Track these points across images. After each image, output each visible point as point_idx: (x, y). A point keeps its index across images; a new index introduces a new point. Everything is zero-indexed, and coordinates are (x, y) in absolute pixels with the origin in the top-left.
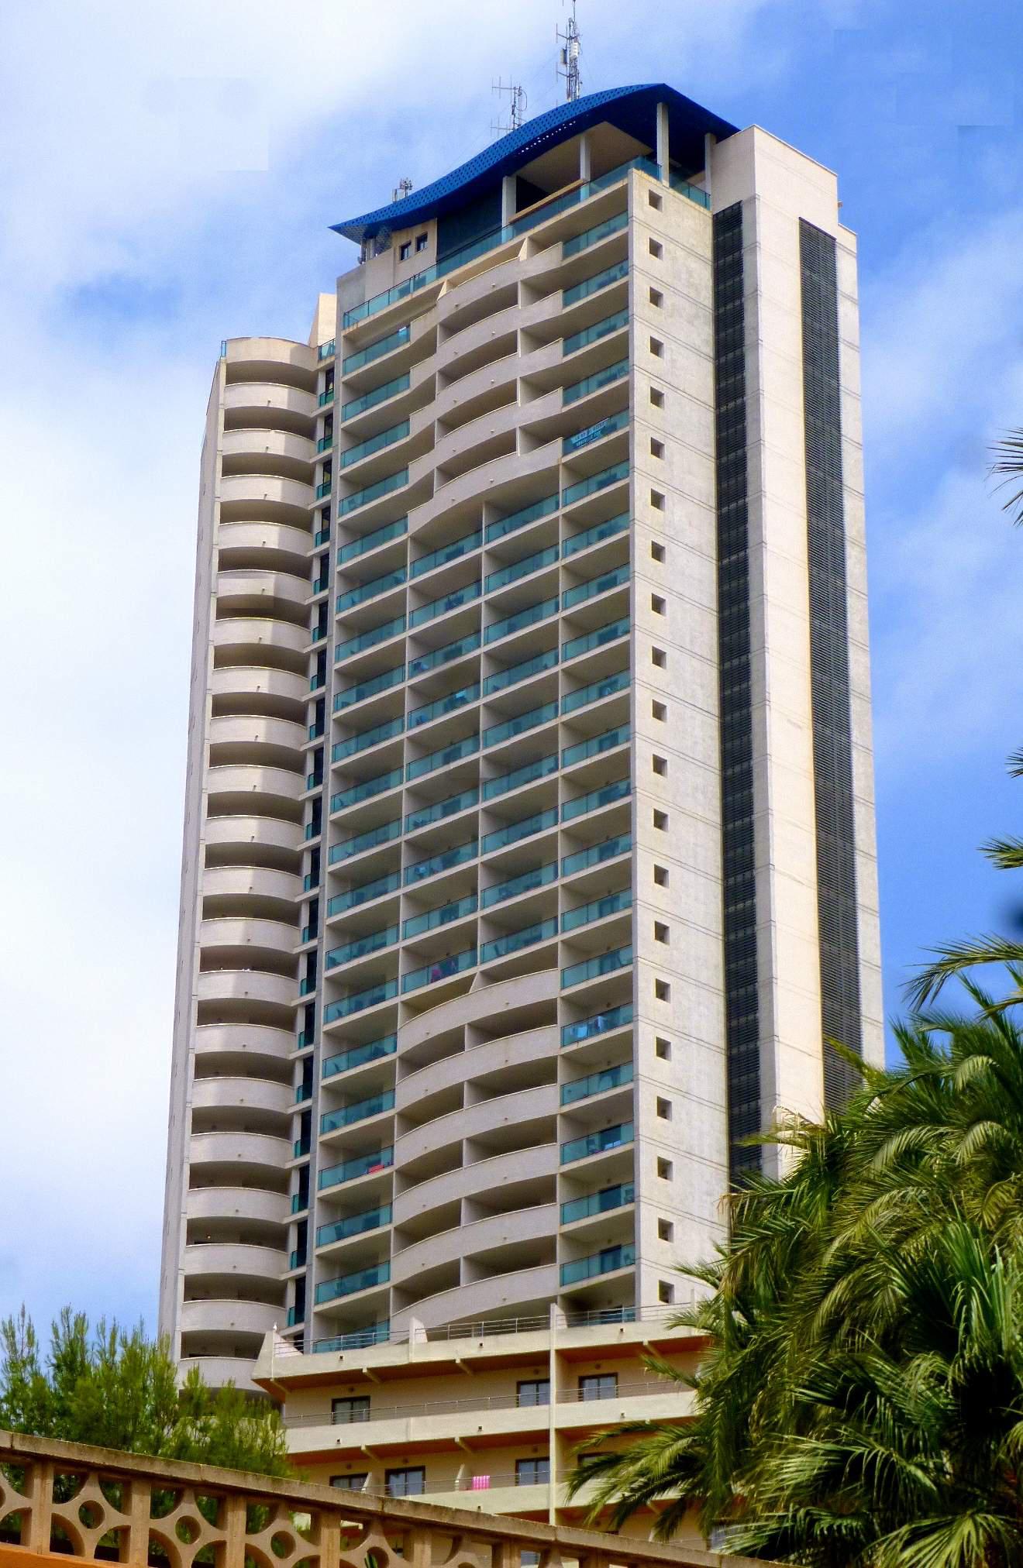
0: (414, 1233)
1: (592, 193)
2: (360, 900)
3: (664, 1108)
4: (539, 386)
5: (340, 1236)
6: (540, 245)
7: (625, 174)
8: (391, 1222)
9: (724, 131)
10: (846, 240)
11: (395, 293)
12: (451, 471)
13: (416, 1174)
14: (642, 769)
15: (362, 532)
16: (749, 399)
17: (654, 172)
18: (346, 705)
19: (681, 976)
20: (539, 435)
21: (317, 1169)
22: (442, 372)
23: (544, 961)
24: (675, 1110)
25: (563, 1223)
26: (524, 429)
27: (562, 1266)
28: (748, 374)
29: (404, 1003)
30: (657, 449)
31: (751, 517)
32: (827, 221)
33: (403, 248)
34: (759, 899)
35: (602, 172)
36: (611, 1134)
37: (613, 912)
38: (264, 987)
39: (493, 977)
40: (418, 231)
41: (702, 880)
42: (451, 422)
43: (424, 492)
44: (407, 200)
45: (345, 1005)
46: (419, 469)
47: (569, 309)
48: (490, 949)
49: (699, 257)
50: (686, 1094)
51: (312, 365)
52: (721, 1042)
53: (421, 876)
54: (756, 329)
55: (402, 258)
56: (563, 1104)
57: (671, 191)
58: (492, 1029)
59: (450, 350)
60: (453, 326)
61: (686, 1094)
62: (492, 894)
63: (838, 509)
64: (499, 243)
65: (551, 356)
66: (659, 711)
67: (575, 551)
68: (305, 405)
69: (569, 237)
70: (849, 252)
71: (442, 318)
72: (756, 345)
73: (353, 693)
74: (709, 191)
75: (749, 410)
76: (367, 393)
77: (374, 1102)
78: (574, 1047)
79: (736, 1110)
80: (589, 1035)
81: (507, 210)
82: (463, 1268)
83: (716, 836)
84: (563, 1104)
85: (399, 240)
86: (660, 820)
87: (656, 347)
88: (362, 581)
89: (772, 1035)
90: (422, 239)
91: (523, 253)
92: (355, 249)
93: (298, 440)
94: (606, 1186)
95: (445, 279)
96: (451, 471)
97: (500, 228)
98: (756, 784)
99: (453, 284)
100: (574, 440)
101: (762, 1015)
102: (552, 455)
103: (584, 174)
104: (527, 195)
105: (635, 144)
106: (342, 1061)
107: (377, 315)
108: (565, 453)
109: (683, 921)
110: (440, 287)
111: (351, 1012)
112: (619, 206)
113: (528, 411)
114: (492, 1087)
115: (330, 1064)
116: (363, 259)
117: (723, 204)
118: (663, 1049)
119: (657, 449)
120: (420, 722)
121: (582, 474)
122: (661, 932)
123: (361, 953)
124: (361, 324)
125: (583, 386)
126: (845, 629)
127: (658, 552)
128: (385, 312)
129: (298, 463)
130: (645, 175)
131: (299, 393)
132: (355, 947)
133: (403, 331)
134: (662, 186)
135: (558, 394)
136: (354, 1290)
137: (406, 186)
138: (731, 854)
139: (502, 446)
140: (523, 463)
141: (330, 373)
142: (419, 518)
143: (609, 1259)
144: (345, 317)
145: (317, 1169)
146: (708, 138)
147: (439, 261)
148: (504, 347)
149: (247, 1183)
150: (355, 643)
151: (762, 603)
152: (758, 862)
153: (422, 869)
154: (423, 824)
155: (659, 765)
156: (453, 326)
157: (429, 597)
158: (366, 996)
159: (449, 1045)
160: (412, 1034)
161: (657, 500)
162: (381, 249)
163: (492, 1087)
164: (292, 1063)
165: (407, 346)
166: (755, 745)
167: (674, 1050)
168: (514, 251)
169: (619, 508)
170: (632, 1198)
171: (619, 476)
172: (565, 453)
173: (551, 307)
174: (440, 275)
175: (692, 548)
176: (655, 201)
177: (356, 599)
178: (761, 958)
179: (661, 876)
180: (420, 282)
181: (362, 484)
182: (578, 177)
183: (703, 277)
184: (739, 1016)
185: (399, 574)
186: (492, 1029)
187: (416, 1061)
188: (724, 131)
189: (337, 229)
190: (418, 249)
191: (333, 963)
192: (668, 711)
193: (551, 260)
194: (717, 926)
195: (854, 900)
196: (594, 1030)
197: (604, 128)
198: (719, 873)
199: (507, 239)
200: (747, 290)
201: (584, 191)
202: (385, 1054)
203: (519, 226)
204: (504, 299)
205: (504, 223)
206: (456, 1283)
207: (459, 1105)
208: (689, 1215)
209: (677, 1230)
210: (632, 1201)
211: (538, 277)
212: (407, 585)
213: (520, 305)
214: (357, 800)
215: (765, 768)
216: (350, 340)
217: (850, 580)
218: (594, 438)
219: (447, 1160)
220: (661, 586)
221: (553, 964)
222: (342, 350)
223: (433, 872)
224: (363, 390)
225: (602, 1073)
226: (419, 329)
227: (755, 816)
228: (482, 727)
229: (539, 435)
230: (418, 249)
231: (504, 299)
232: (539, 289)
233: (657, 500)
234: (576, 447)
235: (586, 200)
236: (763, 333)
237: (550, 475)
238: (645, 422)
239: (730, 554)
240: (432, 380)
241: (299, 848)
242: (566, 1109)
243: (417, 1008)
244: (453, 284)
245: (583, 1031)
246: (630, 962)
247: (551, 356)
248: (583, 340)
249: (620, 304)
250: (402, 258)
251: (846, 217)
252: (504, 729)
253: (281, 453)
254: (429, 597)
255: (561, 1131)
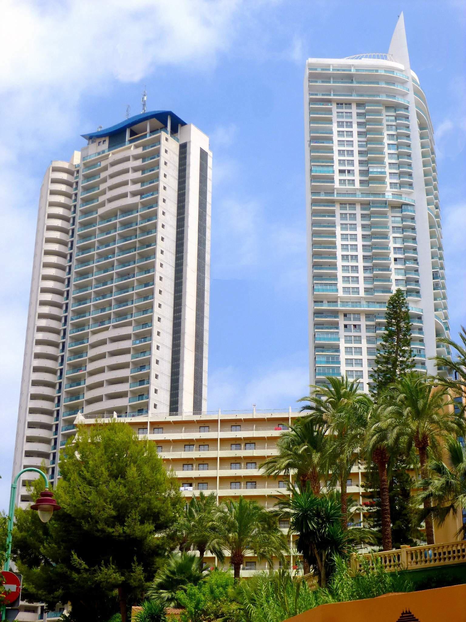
0: (91, 388)
1: (150, 136)
2: (80, 305)
3: (157, 362)
4: (135, 182)
5: (71, 387)
6: (136, 147)
7: (160, 132)
8: (87, 356)
9: (183, 124)
10: (210, 154)
11: (97, 154)
12: (110, 200)
13: (92, 373)
14: (157, 279)
15: (85, 213)
16: (183, 280)
17: (167, 133)
18: (78, 255)
19: (164, 303)
20: (134, 194)
21: (66, 370)
22: (108, 187)
23: (129, 324)
24: (160, 362)
25: (130, 388)
26: (132, 168)
27: (130, 384)
28: (186, 184)
29: (91, 331)
30: (164, 201)
31: (186, 219)
32: (206, 149)
33: (99, 143)
34: (182, 313)
35: (153, 132)
36: (143, 367)
37: (146, 314)
38: (54, 324)
39: (115, 327)
40: (103, 139)
41: (171, 254)
42: (111, 188)
43: (103, 204)
44: (101, 131)
45: (74, 331)
46: (101, 199)
47: (144, 175)
48: (114, 320)
49: (175, 154)
50: (162, 359)
51: (73, 169)
52: (170, 361)
53: (97, 300)
54: (189, 173)
55: (99, 145)
56: (132, 359)
57: (171, 138)
58: (114, 340)
59: (112, 170)
60: (113, 164)
61: (162, 359)
62: (116, 306)
63: (205, 244)
64: (125, 145)
65: (138, 175)
66: (161, 265)
67: (142, 224)
68: (71, 179)
69: (144, 147)
70: (211, 157)
71: (110, 162)
72: (189, 178)
73: (81, 253)
74: (179, 138)
75: (186, 194)
76: (88, 178)
77: (83, 328)
78: (135, 346)
79: (173, 364)
80: (139, 343)
81: (128, 137)
82: (106, 368)
83: (173, 297)
84: (132, 359)
85: (98, 140)
86: (160, 292)
87: (165, 176)
88: (84, 225)
89: (184, 346)
90: (104, 141)
91: (132, 148)
92: (86, 141)
93: (68, 199)
94: (142, 365)
95: (111, 152)
96: (110, 200)
97: (125, 141)
98: (186, 196)
99: (113, 154)
100: (143, 196)
101: (181, 341)
102: (137, 199)
103: (148, 130)
104: (133, 133)
105: (162, 125)
106: (78, 278)
107: (92, 159)
108: (141, 199)
109: (164, 317)
110: (109, 155)
111: (76, 332)
112: (158, 141)
113: (132, 188)
114: (113, 354)
115: (72, 331)
116: (88, 144)
117: (182, 142)
118: (158, 348)
119: (164, 201)
120: (98, 262)
121: (145, 205)
122: (159, 319)
123: (79, 318)
124: (88, 160)
125: (147, 147)
126: (205, 249)
127: (163, 226)
128: (94, 158)
129: (66, 229)
130: (165, 133)
131: (68, 187)
132: (78, 316)
133: (99, 163)
134: (169, 136)
135: (139, 184)
136: (73, 400)
137: (101, 127)
138: (176, 302)
139: (125, 196)
140: (129, 201)
141: (78, 172)
142: (101, 211)
143: (141, 397)
144: (83, 158)
145: (66, 370)
146: (179, 125)
147: (109, 147)
148: (126, 171)
149: (48, 345)
150: (83, 228)
151: (187, 241)
152: (180, 388)
153: (97, 298)
154: (98, 287)
155: (161, 279)
156: (113, 164)
157: (102, 231)
158: (80, 329)
159: (103, 342)
160: (93, 339)
161: (164, 213)
162: (93, 142)
163: (113, 354)
164: (63, 304)
165: (100, 167)
166: (186, 187)
167: (160, 348)
168: (130, 148)
169: (150, 307)
170: (148, 383)
171: (154, 206)
172: (141, 199)
173: (139, 163)
174: (109, 151)
175: (172, 176)
176: (167, 139)
177: (72, 359)
178: (182, 327)
179: (160, 306)
180: (103, 152)
181: (86, 201)
182: (146, 131)
183: (177, 159)
184: (178, 267)
185: (94, 224)
186: (114, 340)
187: (93, 346)
188: (183, 124)
189: (81, 136)
190: (103, 143)
191: (72, 319)
192: (164, 252)
193: (140, 151)
194: (172, 319)
195: (204, 314)
196: (141, 342)
197: (154, 120)
198: (173, 306)
199: (127, 145)
200: (187, 163)
201: (148, 135)
202: (85, 343)
203: (131, 141)
204: (127, 159)
205: (127, 140)
206: (102, 400)
207: (105, 357)
208: (161, 388)
209: (159, 391)
210: (149, 384)
211: (135, 155)
212: (97, 227)
213: (131, 161)
214: (80, 280)
215: (186, 282)
216: (84, 164)
217: (207, 237)
218: (148, 196)
219: (101, 371)
220: (165, 209)
221: (131, 325)
222: (82, 167)
223: (100, 299)
224: (87, 177)
225: (141, 352)
226: (103, 164)
227: (182, 313)
228: (114, 291)
229: (134, 194)
230: (103, 143)
231: (127, 159)
232: (136, 158)
233: (164, 213)
234: (143, 198)
235: (148, 138)
236: (191, 163)
237: (136, 205)
238: (163, 170)
239: (180, 215)
240: (106, 177)
241: (70, 216)
242: (133, 360)
243: (94, 333)
244: (113, 154)
245: (138, 342)
246: (151, 326)
247: (138, 175)
248: (146, 160)
249: (157, 164)
250: (99, 145)
251: (211, 148)
252: (121, 266)
253: (64, 190)
254: (102, 231)
255: (129, 395)
